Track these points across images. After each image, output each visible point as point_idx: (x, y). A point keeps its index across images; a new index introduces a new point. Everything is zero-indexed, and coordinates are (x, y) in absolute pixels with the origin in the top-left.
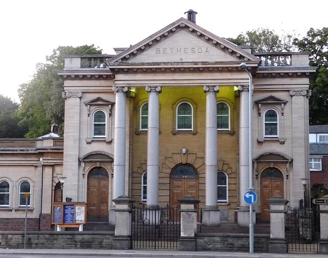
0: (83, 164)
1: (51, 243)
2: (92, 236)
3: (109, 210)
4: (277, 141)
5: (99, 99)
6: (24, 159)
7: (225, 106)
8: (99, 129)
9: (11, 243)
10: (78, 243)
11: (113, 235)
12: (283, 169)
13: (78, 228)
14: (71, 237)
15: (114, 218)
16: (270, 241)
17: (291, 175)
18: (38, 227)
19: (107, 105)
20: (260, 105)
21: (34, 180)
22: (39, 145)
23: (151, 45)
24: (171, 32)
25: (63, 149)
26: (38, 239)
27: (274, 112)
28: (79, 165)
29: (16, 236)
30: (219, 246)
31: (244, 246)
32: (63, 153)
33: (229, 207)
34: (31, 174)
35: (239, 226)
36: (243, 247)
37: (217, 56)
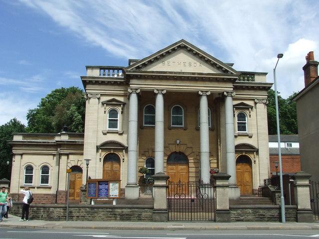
1: (49, 213)
2: (129, 210)
4: (246, 135)
5: (113, 100)
6: (44, 149)
8: (113, 124)
9: (52, 216)
11: (152, 208)
12: (251, 156)
14: (111, 210)
19: (120, 105)
22: (57, 139)
24: (174, 50)
28: (97, 151)
29: (58, 209)
30: (250, 217)
34: (49, 161)
37: (206, 70)
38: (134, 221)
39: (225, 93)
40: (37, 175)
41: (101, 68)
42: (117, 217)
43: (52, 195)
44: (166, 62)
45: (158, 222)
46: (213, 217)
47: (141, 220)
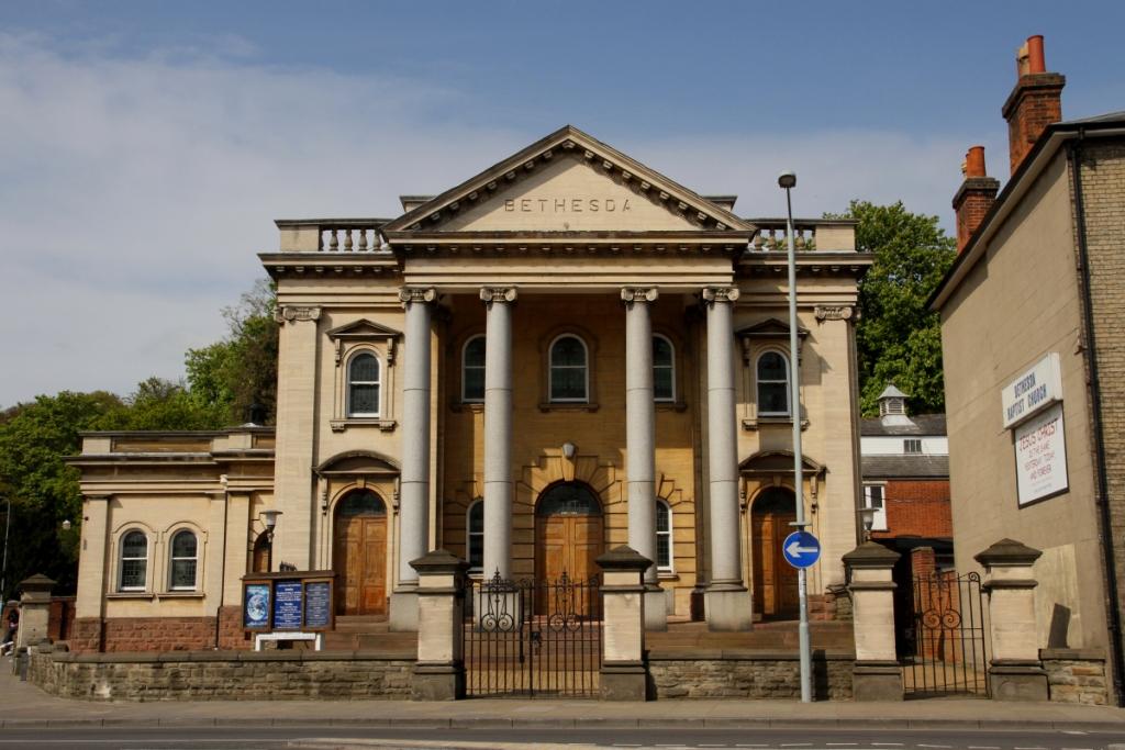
0: (322, 484)
1: (237, 685)
3: (388, 593)
5: (363, 325)
7: (663, 345)
8: (362, 397)
10: (315, 685)
13: (313, 641)
15: (402, 613)
16: (856, 670)
17: (822, 502)
18: (214, 638)
19: (383, 340)
20: (747, 341)
21: (207, 527)
22: (219, 445)
23: (495, 190)
24: (542, 161)
25: (273, 455)
26: (200, 674)
27: (779, 357)
28: (314, 485)
30: (709, 685)
31: (782, 685)
32: (272, 464)
33: (676, 584)
35: (712, 628)
36: (777, 688)
37: (495, 220)
38: (361, 697)
39: (623, 295)
40: (157, 560)
41: (324, 226)
42: (311, 688)
43: (208, 619)
44: (518, 201)
45: (431, 699)
46: (981, 684)
47: (381, 694)
